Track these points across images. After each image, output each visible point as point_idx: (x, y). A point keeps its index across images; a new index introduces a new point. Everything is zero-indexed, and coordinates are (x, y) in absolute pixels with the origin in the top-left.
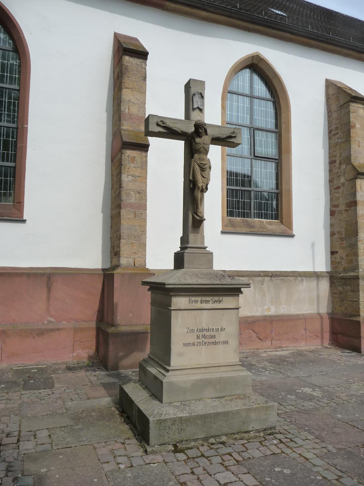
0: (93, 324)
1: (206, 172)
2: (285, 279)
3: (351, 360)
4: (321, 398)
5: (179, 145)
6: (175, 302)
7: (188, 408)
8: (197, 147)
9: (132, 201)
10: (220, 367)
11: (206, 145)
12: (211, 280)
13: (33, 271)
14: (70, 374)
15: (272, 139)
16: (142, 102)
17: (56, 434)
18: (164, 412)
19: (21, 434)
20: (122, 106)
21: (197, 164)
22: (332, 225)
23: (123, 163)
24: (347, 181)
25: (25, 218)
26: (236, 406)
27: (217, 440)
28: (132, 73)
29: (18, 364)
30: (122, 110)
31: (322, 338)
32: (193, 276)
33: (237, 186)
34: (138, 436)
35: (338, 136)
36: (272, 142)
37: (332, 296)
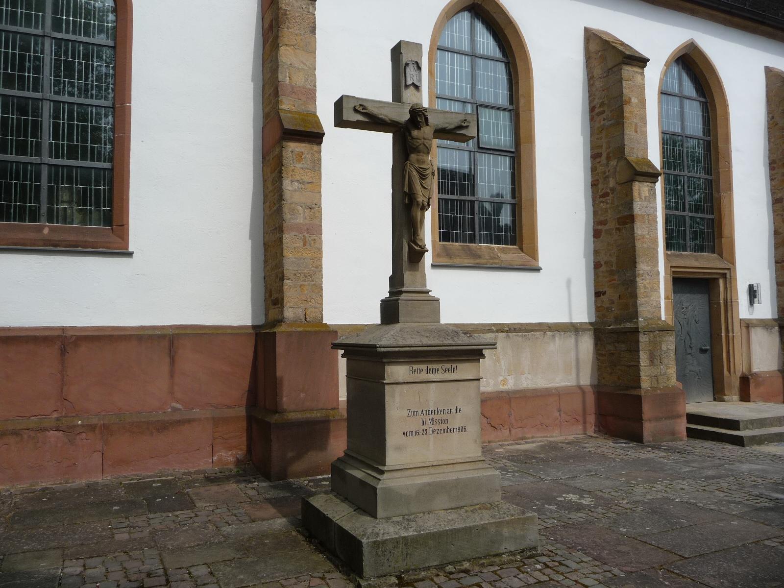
0: (242, 412)
1: (427, 180)
2: (528, 335)
3: (629, 453)
4: (594, 507)
5: (385, 140)
6: (389, 372)
7: (414, 524)
8: (415, 143)
9: (300, 220)
10: (456, 465)
11: (427, 141)
12: (441, 339)
13: (147, 332)
14: (214, 488)
15: (504, 120)
16: (311, 67)
17: (221, 571)
18: (382, 531)
19: (169, 572)
20: (279, 74)
21: (414, 168)
22: (596, 252)
23: (284, 162)
24: (619, 184)
25: (130, 249)
26: (481, 519)
27: (456, 567)
28: (294, 21)
29: (129, 475)
30: (279, 80)
31: (585, 422)
32: (414, 334)
33: (452, 194)
34: (342, 567)
35: (604, 116)
36: (504, 125)
37: (598, 359)
